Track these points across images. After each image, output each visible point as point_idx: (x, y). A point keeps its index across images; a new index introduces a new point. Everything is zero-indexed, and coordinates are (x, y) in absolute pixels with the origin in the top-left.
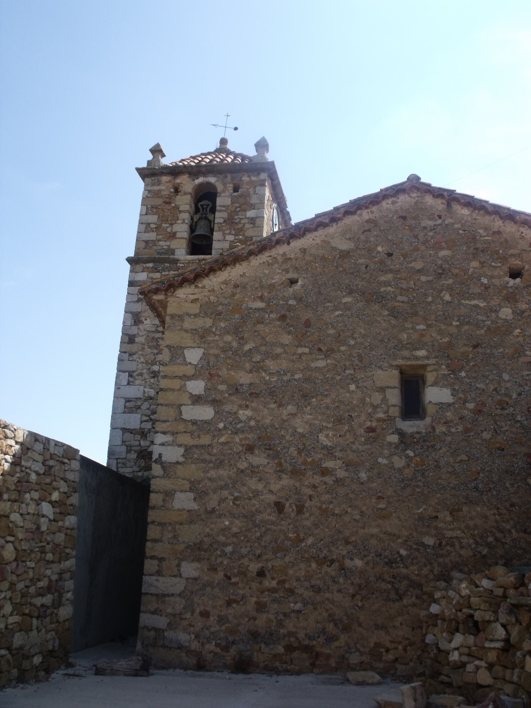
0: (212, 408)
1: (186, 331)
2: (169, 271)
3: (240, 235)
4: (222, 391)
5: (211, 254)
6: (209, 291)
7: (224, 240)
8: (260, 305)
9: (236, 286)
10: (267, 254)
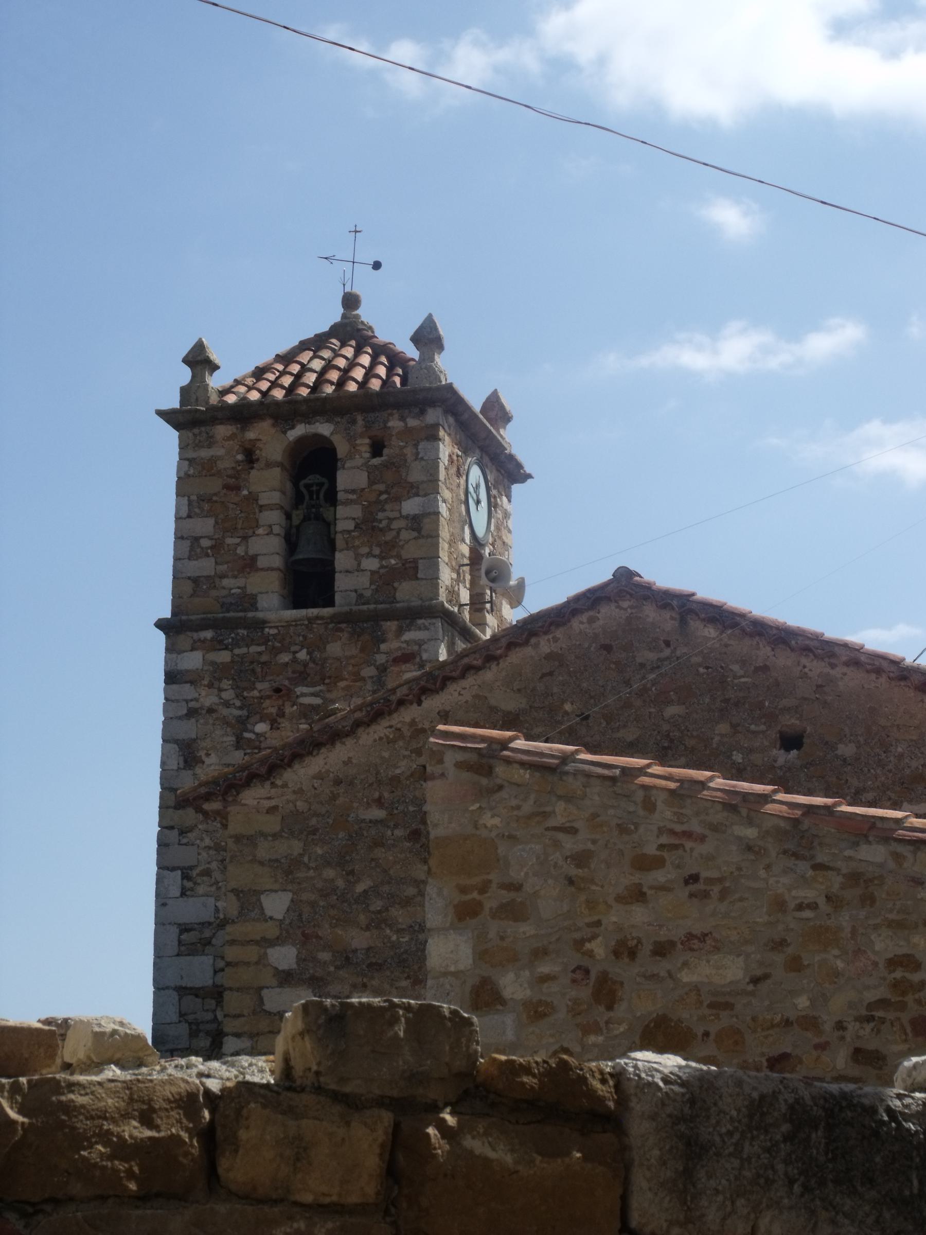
0: (311, 990)
1: (261, 863)
2: (248, 646)
3: (392, 557)
4: (325, 963)
5: (330, 603)
6: (294, 792)
7: (359, 569)
8: (378, 813)
9: (338, 782)
10: (385, 723)
